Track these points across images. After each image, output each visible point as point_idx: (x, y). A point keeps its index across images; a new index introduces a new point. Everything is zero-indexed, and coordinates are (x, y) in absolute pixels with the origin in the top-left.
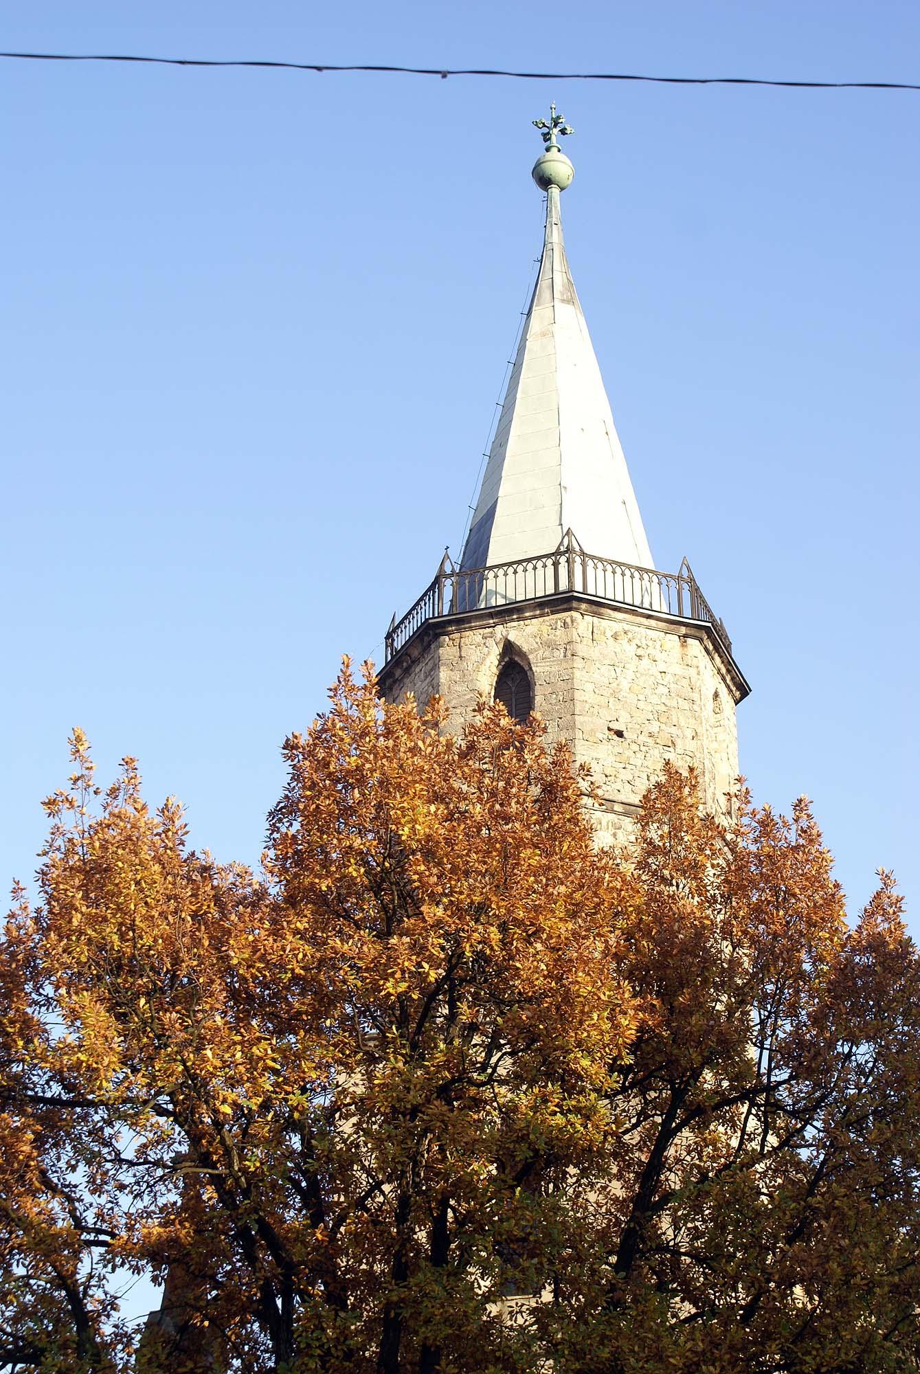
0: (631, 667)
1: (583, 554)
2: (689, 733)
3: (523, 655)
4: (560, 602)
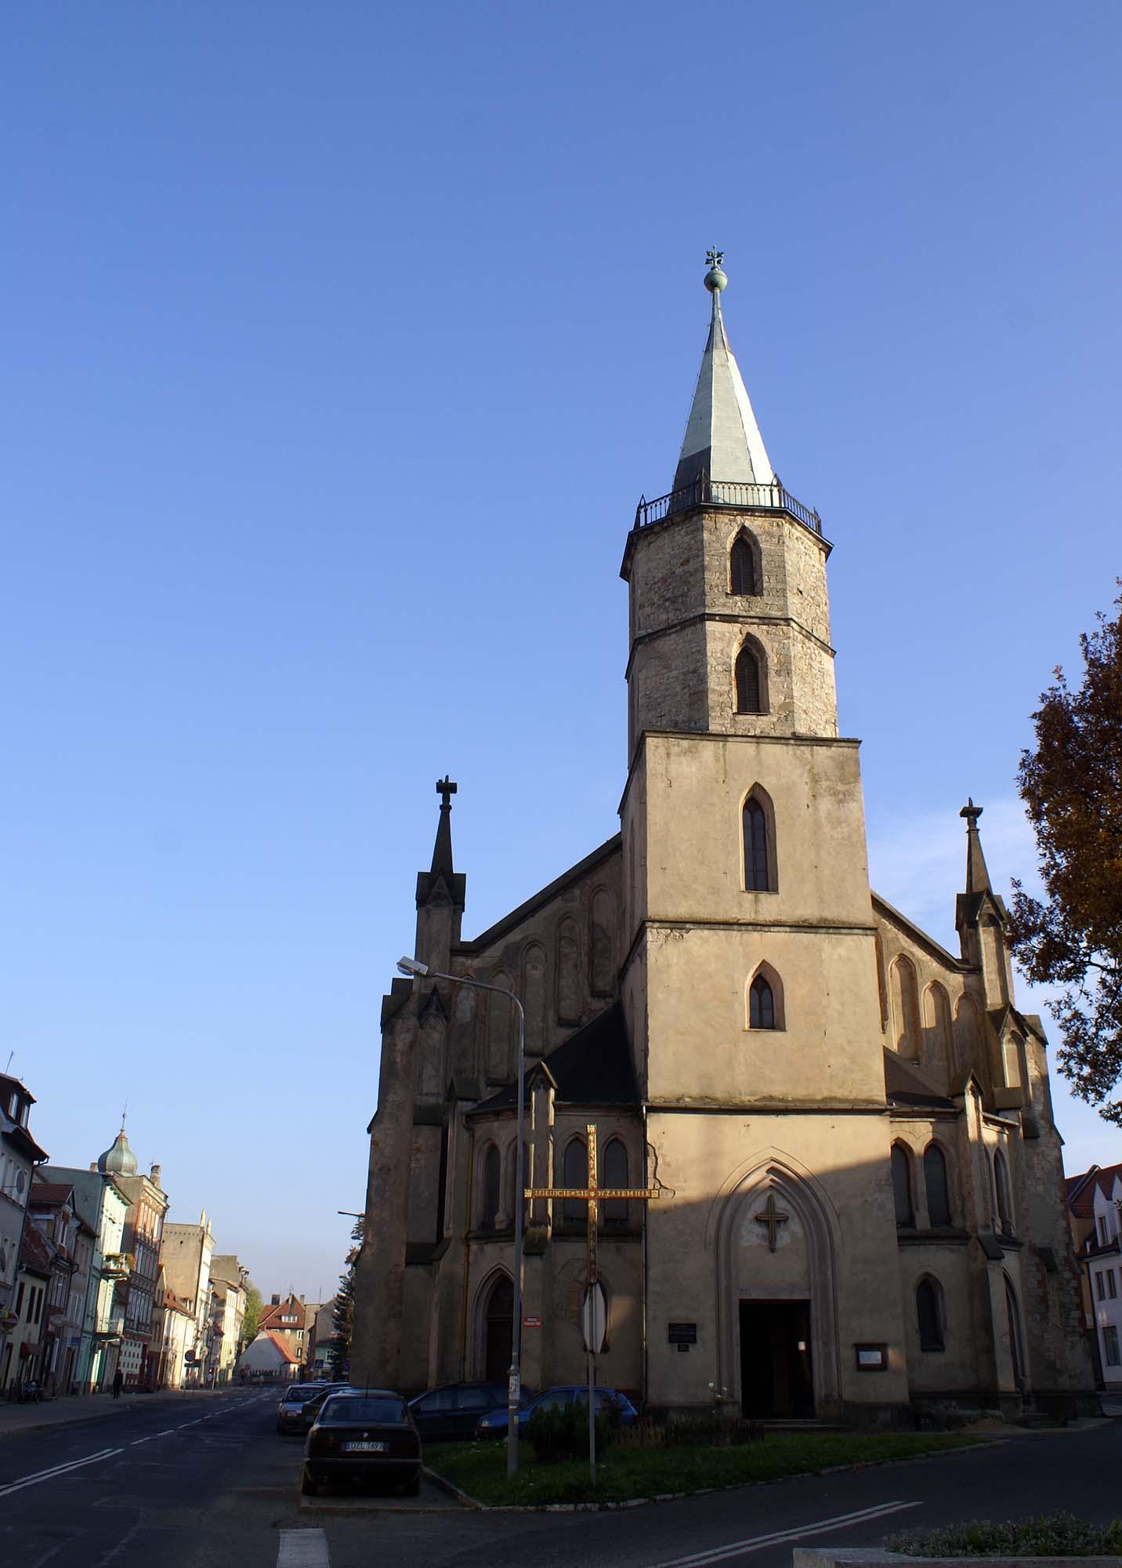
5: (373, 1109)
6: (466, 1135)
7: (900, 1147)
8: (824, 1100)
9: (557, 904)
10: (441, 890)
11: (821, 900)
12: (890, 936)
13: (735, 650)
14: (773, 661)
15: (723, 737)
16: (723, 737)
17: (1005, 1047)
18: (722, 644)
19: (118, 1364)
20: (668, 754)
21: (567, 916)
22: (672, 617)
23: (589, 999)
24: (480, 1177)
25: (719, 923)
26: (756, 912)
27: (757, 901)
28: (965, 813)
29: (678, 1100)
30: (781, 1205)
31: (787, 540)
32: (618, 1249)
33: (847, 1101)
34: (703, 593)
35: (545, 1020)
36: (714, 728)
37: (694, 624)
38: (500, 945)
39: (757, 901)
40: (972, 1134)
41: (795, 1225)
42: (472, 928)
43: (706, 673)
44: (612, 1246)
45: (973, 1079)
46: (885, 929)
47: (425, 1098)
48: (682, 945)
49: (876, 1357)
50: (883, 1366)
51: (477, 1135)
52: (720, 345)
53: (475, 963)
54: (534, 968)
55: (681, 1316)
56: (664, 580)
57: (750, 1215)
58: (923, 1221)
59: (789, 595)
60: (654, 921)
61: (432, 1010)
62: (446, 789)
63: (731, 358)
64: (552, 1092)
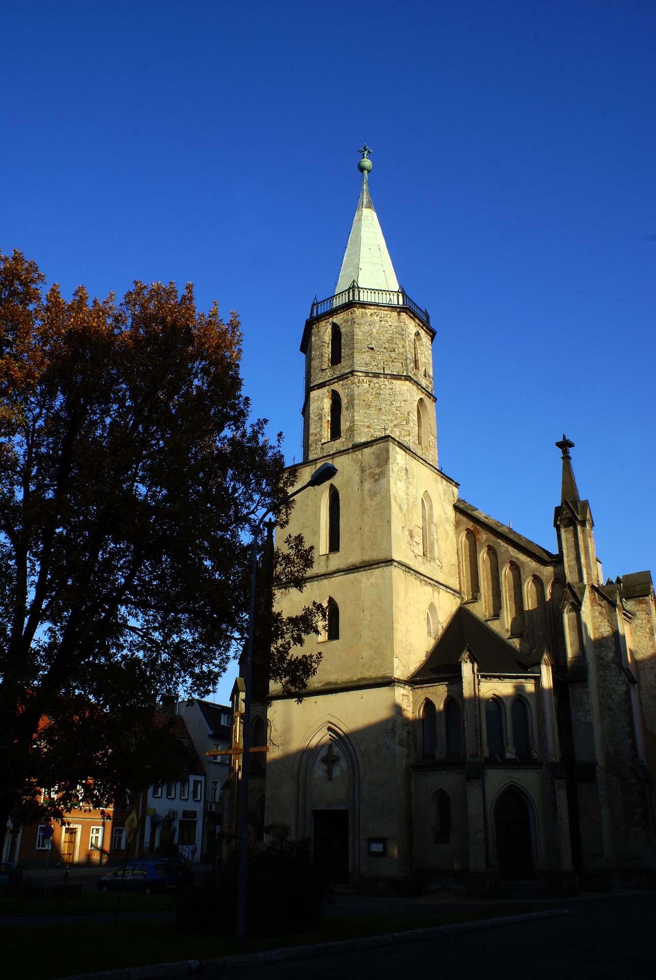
0: (377, 326)
1: (358, 287)
2: (400, 346)
3: (338, 326)
4: (349, 305)
7: (429, 704)
8: (359, 680)
11: (363, 549)
12: (503, 549)
17: (566, 617)
28: (560, 445)
30: (336, 750)
40: (467, 691)
41: (343, 764)
45: (469, 650)
46: (500, 545)
48: (289, 597)
49: (377, 847)
50: (384, 854)
57: (319, 758)
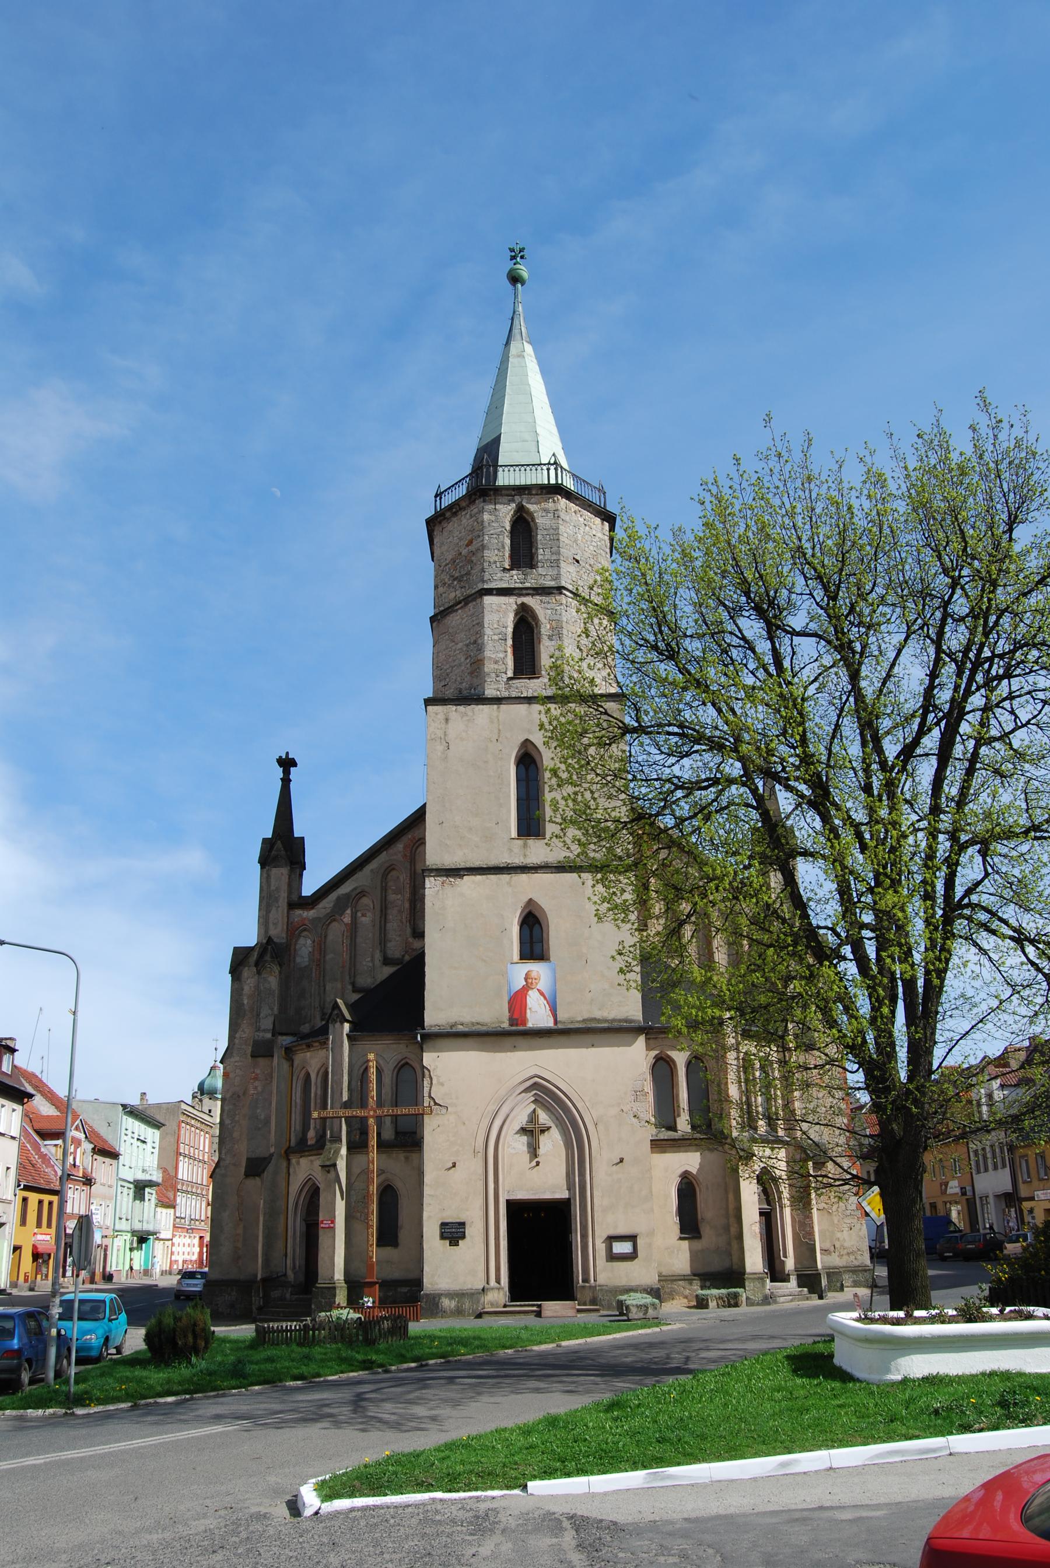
5: (223, 1045)
6: (286, 1065)
9: (383, 857)
10: (283, 850)
13: (510, 621)
14: (545, 629)
15: (498, 701)
16: (498, 701)
18: (499, 616)
19: (172, 1253)
20: (447, 720)
21: (390, 868)
22: (459, 594)
23: (411, 940)
24: (298, 1101)
25: (503, 868)
26: (525, 856)
27: (525, 846)
29: (451, 1027)
31: (562, 515)
32: (407, 1158)
33: (606, 1021)
34: (483, 570)
35: (372, 961)
36: (490, 692)
37: (474, 600)
38: (333, 896)
39: (525, 846)
42: (311, 883)
43: (483, 644)
44: (402, 1156)
47: (261, 1034)
51: (296, 1063)
52: (518, 337)
53: (311, 914)
54: (363, 915)
55: (451, 1217)
56: (453, 561)
58: (683, 1123)
59: (562, 564)
60: (432, 870)
61: (268, 958)
62: (287, 764)
63: (529, 349)
64: (347, 1026)
